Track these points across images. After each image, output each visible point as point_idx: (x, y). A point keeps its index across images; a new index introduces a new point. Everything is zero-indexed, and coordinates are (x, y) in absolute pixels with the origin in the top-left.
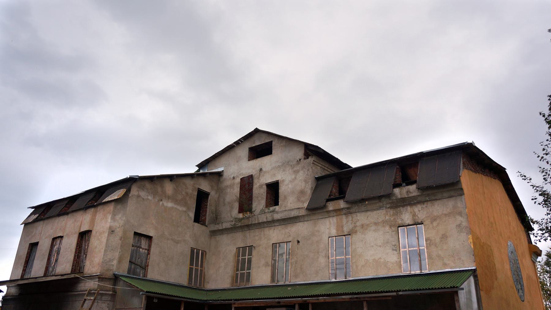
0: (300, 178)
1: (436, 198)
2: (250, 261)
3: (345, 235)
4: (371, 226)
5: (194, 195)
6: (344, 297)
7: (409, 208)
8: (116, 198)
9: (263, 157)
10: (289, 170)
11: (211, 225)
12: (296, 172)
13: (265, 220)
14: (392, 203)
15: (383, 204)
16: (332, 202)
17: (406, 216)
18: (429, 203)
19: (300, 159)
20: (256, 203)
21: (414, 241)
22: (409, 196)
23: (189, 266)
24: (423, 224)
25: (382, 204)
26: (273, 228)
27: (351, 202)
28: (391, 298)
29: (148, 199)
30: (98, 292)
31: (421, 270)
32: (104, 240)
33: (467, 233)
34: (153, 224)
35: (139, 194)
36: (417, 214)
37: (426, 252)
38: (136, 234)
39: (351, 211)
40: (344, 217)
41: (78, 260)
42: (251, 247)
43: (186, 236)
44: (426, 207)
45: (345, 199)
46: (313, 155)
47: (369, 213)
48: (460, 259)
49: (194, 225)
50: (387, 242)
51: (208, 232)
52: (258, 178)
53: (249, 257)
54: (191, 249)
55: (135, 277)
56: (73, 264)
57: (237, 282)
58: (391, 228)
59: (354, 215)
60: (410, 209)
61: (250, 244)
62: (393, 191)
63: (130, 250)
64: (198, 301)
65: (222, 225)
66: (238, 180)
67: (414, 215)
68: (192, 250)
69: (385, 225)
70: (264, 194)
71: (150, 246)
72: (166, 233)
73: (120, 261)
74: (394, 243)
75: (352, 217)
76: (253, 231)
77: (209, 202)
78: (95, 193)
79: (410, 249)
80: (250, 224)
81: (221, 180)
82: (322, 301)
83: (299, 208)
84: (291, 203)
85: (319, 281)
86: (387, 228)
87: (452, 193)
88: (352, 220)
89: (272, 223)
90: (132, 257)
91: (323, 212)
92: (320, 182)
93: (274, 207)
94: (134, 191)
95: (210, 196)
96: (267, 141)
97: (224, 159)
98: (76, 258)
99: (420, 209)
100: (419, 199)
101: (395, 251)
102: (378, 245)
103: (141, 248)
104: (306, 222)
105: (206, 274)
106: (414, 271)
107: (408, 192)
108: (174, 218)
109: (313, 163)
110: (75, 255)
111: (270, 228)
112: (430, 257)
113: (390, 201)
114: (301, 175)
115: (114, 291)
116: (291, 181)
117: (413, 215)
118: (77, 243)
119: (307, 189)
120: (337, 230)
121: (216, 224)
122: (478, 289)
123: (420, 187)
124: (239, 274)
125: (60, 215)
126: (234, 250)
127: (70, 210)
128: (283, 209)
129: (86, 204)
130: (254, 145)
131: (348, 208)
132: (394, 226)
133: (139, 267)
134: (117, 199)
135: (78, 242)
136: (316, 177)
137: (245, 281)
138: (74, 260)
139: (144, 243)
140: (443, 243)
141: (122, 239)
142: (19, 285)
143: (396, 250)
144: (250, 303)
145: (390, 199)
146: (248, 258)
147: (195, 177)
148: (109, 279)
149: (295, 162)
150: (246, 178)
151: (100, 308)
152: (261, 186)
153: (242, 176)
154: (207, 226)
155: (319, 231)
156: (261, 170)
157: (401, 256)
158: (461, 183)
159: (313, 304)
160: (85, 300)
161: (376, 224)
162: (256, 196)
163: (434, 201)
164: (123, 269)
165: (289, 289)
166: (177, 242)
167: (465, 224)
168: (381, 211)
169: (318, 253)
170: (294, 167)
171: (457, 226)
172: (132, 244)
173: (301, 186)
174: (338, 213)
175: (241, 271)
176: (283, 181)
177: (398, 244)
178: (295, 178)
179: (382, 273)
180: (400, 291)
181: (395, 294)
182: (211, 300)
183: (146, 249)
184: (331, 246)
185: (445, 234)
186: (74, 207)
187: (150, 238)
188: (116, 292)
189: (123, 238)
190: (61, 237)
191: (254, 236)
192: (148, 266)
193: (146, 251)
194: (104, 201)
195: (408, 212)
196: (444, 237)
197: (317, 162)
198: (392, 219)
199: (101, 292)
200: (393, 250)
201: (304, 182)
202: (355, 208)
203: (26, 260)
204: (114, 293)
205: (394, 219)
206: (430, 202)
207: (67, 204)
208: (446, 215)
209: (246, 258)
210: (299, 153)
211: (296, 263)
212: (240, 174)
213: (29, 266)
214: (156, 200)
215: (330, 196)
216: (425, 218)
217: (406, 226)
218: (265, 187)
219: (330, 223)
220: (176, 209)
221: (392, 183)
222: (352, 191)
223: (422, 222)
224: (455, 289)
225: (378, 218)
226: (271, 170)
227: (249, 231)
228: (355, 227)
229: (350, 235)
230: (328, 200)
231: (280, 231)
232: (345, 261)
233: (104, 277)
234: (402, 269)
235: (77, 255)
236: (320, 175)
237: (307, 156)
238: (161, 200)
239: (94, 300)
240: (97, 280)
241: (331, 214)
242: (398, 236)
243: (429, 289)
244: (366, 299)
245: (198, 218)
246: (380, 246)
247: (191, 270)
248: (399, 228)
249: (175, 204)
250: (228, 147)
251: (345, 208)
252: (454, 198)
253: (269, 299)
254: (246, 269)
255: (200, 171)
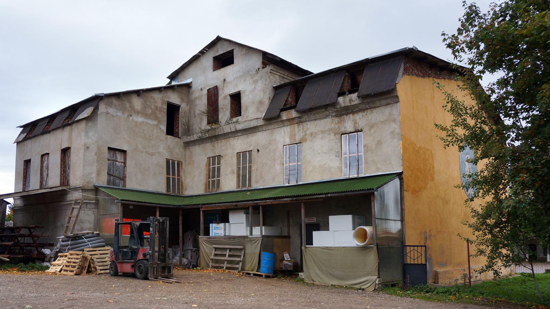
0: (259, 89)
1: (375, 105)
2: (219, 169)
3: (297, 144)
4: (319, 134)
5: (164, 108)
6: (286, 199)
7: (351, 116)
8: (86, 116)
9: (226, 67)
10: (249, 80)
11: (184, 137)
12: (256, 82)
13: (229, 131)
14: (337, 111)
15: (329, 113)
16: (285, 112)
17: (349, 124)
18: (369, 110)
19: (259, 68)
20: (222, 114)
21: (354, 147)
22: (351, 104)
23: (166, 176)
24: (362, 131)
25: (328, 112)
26: (237, 138)
27: (301, 112)
28: (322, 200)
29: (117, 115)
30: (82, 201)
31: (358, 174)
32: (81, 156)
33: (398, 139)
34: (125, 139)
35: (107, 111)
36: (357, 122)
37: (363, 158)
38: (110, 149)
39: (302, 120)
40: (296, 126)
41: (64, 174)
42: (219, 157)
43: (160, 148)
44: (366, 114)
45: (297, 109)
46: (270, 64)
47: (317, 122)
48: (390, 163)
49: (167, 137)
50: (332, 149)
51: (182, 143)
52: (223, 89)
53: (218, 166)
54: (167, 160)
55: (115, 187)
56: (60, 177)
57: (209, 188)
58: (335, 136)
59: (305, 124)
60: (352, 116)
61: (218, 154)
62: (337, 99)
63: (107, 165)
64: (171, 206)
65: (193, 137)
66: (205, 92)
67: (355, 123)
68: (168, 161)
69: (330, 133)
70: (228, 105)
71: (125, 159)
72: (140, 147)
73: (98, 174)
74: (337, 150)
75: (303, 126)
76: (220, 141)
77: (180, 114)
78: (69, 111)
79: (350, 155)
80: (217, 134)
81: (191, 91)
82: (270, 203)
83: (257, 119)
84: (251, 114)
85: (275, 186)
86: (332, 136)
87: (389, 101)
88: (303, 129)
89: (235, 133)
90: (109, 170)
91: (278, 121)
92: (278, 91)
93: (237, 118)
94: (102, 107)
95: (181, 108)
96: (229, 49)
97: (192, 70)
98: (63, 172)
99: (361, 118)
100: (360, 107)
101: (338, 157)
102: (324, 151)
103: (117, 161)
104: (264, 131)
105: (184, 181)
106: (352, 175)
107: (351, 100)
108: (146, 132)
109: (270, 72)
110: (61, 170)
111: (235, 138)
112: (366, 162)
113: (335, 110)
114: (260, 85)
115: (97, 201)
116: (252, 91)
117: (354, 123)
118: (61, 159)
119: (265, 99)
120: (291, 139)
121: (188, 136)
122: (403, 190)
123: (360, 95)
124: (211, 181)
125: (64, 126)
126: (206, 160)
127: (51, 128)
128: (245, 119)
129: (63, 123)
130: (217, 54)
131: (299, 118)
132: (338, 133)
133: (118, 179)
134: (86, 117)
135: (61, 158)
136: (274, 86)
137: (216, 188)
138: (61, 174)
139: (119, 157)
140: (378, 149)
141: (97, 154)
142: (22, 197)
143: (338, 156)
144: (214, 206)
145: (335, 108)
146: (217, 167)
147: (162, 91)
148: (91, 190)
149: (254, 72)
150: (211, 90)
151: (87, 214)
152: (225, 97)
153: (209, 87)
154: (180, 138)
155: (275, 140)
156: (225, 80)
157: (343, 162)
158: (396, 90)
159: (263, 206)
160: (73, 208)
161: (323, 132)
162: (222, 107)
163: (373, 109)
164: (103, 181)
165: (248, 193)
166: (152, 154)
167: (397, 130)
168: (328, 119)
169: (275, 160)
170: (253, 77)
171: (390, 133)
172: (108, 158)
173: (260, 96)
174: (292, 122)
175: (212, 178)
176: (244, 91)
177: (341, 151)
178: (255, 88)
179: (327, 177)
180: (329, 193)
181: (324, 196)
182: (183, 205)
183: (122, 162)
184: (285, 154)
185: (380, 141)
186: (53, 126)
187: (124, 152)
188: (99, 201)
189: (99, 153)
190: (48, 154)
191: (221, 146)
192: (126, 177)
193: (123, 164)
194: (76, 119)
195: (350, 120)
196: (379, 143)
197: (275, 71)
198: (337, 127)
199: (84, 201)
200: (336, 156)
201: (262, 93)
202: (305, 117)
203: (24, 176)
204: (97, 202)
205: (339, 127)
206: (370, 110)
207: (48, 123)
208: (382, 122)
209: (215, 167)
210: (257, 61)
211: (257, 170)
212: (207, 85)
213: (27, 181)
214: (126, 116)
215: (285, 105)
216: (364, 125)
217: (349, 133)
218: (229, 98)
219: (285, 132)
220: (147, 123)
221: (338, 92)
222: (305, 102)
223: (361, 129)
224: (372, 191)
225: (325, 127)
226: (234, 80)
227: (216, 142)
228: (306, 135)
229: (301, 143)
230: (282, 110)
231: (243, 140)
232: (296, 167)
233: (86, 188)
234: (343, 173)
235: (62, 170)
236: (278, 84)
237: (264, 65)
238: (131, 116)
239: (80, 208)
240: (81, 191)
241: (286, 123)
242: (340, 141)
243: (351, 191)
244: (304, 201)
245: (171, 130)
246: (326, 153)
247: (168, 179)
248: (342, 136)
249: (145, 118)
250: (194, 57)
251: (297, 117)
252: (390, 105)
253: (228, 202)
254: (216, 176)
255: (171, 83)
